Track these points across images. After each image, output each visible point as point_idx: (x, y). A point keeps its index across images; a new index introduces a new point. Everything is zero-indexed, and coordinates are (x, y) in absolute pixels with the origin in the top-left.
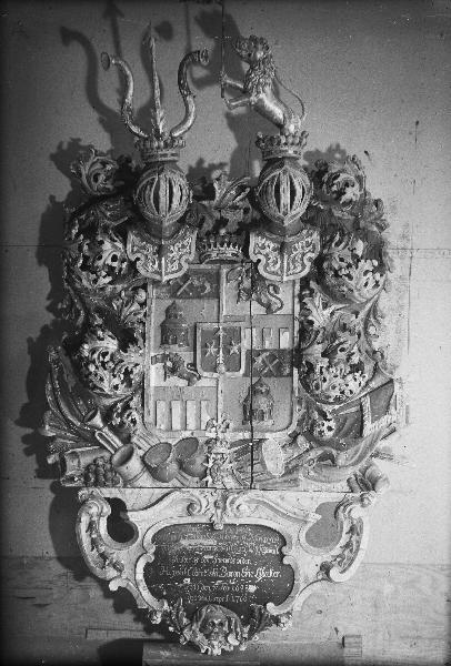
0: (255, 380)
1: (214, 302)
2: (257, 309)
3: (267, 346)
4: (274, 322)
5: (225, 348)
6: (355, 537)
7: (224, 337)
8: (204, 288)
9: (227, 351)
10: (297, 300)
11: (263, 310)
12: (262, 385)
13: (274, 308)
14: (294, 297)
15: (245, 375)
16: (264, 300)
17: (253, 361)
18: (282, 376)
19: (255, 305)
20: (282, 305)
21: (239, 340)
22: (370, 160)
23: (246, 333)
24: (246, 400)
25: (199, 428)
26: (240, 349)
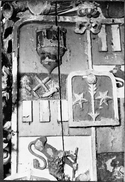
0: (56, 71)
1: (99, 152)
2: (55, 142)
3: (45, 102)
4: (38, 129)
5: (89, 98)
6: (14, 154)
7: (89, 110)
8: (114, 164)
9: (86, 95)
10: (15, 147)
11: (50, 141)
12: (49, 63)
13: (39, 144)
14: (18, 132)
15: (66, 76)
16: (50, 151)
17: (59, 90)
18: (29, 75)
19: (59, 148)
20: (50, 121)
21: (75, 106)
22: (53, 105)
23: (68, 115)
24: (65, 51)
25: (108, 26)
26: (74, 98)
